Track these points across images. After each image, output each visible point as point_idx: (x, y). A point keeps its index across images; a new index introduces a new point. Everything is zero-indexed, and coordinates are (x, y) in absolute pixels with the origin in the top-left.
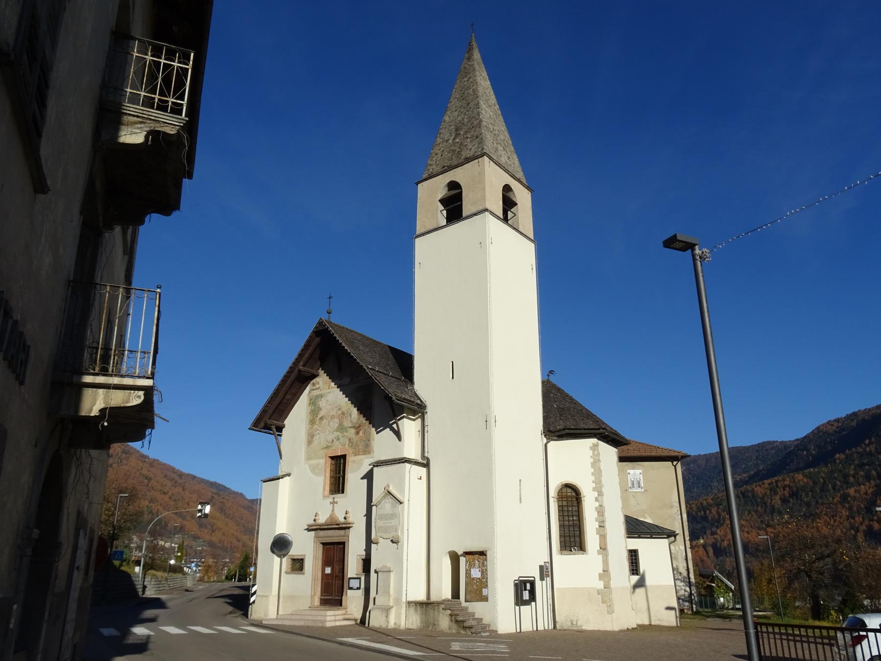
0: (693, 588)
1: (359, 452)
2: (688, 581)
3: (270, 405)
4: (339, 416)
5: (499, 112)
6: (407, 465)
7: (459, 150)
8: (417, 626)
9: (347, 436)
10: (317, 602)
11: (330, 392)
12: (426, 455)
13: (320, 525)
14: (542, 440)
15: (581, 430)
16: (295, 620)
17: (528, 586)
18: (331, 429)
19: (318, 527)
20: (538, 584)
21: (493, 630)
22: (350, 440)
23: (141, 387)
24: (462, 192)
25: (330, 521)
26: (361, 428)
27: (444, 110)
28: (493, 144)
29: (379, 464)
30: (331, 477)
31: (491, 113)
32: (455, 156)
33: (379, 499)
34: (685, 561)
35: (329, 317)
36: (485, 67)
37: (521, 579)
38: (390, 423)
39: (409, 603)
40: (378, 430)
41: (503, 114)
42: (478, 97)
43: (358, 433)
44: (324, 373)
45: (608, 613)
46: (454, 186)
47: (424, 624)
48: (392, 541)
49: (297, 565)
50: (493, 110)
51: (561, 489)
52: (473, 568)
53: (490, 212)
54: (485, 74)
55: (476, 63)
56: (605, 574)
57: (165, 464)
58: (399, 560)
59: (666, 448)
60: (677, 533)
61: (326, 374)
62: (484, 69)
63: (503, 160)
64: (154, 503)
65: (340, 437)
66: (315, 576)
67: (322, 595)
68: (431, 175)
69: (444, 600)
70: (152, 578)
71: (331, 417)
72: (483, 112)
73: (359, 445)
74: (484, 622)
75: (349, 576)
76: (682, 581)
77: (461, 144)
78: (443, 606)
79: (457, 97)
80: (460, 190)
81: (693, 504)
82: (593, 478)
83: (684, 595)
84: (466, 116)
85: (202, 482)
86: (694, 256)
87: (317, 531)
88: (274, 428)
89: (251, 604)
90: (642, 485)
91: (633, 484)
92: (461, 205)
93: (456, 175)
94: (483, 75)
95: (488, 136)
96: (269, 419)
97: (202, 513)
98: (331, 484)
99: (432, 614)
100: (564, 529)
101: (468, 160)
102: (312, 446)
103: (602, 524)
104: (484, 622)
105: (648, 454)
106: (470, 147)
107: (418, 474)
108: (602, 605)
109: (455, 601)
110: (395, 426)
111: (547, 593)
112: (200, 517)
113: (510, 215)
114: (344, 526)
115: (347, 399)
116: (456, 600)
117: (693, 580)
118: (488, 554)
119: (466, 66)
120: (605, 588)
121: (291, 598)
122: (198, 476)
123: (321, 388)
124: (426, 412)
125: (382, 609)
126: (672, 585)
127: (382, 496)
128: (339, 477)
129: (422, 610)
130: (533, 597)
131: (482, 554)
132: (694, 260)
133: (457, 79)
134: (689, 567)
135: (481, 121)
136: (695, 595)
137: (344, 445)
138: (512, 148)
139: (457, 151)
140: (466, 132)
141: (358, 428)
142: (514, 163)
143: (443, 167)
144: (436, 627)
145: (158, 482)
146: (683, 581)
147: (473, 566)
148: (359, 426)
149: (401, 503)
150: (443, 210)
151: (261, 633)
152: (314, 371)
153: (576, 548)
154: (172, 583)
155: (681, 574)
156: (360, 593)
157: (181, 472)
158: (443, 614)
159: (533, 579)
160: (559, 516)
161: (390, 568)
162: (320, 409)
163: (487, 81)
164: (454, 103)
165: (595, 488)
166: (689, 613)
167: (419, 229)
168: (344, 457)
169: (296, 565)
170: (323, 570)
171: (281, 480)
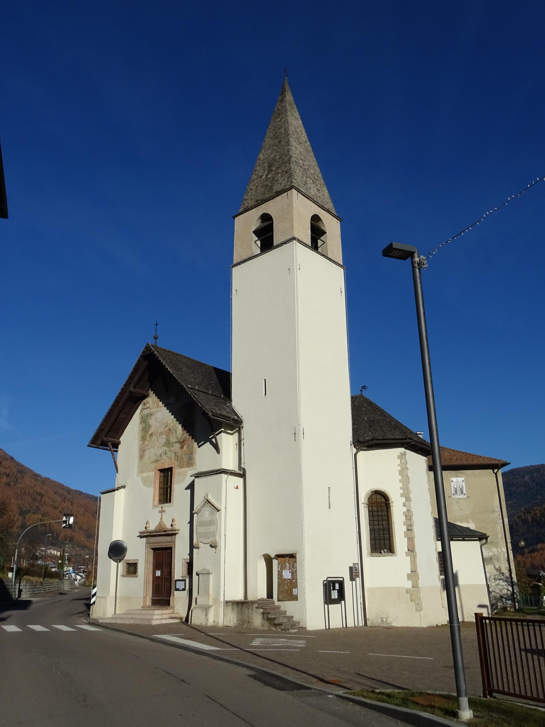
0: (516, 587)
1: (183, 465)
2: (510, 580)
3: (105, 424)
4: (167, 432)
5: (310, 149)
6: (224, 476)
7: (271, 184)
8: (234, 623)
9: (173, 450)
10: (149, 602)
11: (158, 411)
12: (243, 466)
13: (150, 532)
14: (352, 450)
15: (389, 440)
16: (126, 618)
17: (337, 586)
18: (160, 444)
19: (148, 534)
20: (348, 585)
21: (302, 627)
22: (175, 453)
23: (396, 447)
24: (273, 222)
25: (158, 529)
26: (185, 442)
27: (259, 149)
28: (303, 178)
29: (199, 475)
30: (160, 488)
31: (302, 150)
32: (267, 191)
33: (199, 507)
34: (507, 562)
35: (156, 342)
36: (297, 108)
37: (329, 579)
38: (210, 437)
39: (227, 602)
40: (199, 444)
41: (314, 150)
42: (288, 135)
43: (182, 447)
44: (153, 394)
45: (417, 610)
46: (266, 218)
47: (240, 622)
48: (211, 546)
49: (131, 568)
50: (303, 147)
51: (371, 496)
52: (284, 570)
53: (298, 240)
54: (297, 114)
55: (288, 105)
56: (413, 574)
57: (55, 482)
58: (217, 563)
59: (487, 457)
60: (487, 535)
61: (155, 394)
62: (296, 109)
63: (313, 192)
64: (46, 517)
65: (167, 451)
66: (147, 579)
67: (153, 596)
68: (247, 209)
69: (259, 600)
70: (27, 583)
71: (160, 434)
72: (293, 149)
73: (183, 458)
74: (294, 619)
75: (175, 579)
76: (504, 581)
77: (273, 179)
78: (256, 605)
79: (271, 136)
80: (271, 222)
81: (537, 510)
82: (218, 474)
83: (507, 594)
84: (278, 153)
85: (88, 497)
86: (413, 263)
87: (147, 538)
88: (110, 444)
89: (92, 605)
90: (465, 492)
91: (456, 491)
92: (273, 235)
93: (268, 208)
94: (295, 115)
95: (298, 171)
96: (106, 437)
97: (66, 524)
98: (160, 494)
99: (246, 613)
100: (374, 532)
101: (279, 193)
102: (143, 460)
103: (409, 528)
104: (294, 619)
105: (470, 462)
106: (280, 182)
107: (234, 483)
108: (410, 603)
109: (269, 600)
110: (213, 440)
111: (356, 592)
112: (65, 527)
113: (320, 243)
114: (170, 532)
115: (173, 416)
116: (270, 599)
117: (515, 579)
118: (297, 556)
119: (280, 107)
120: (413, 587)
121: (127, 599)
122: (84, 491)
123: (151, 407)
124: (243, 427)
125: (202, 608)
126: (485, 584)
127: (202, 504)
128: (167, 488)
129: (239, 609)
130: (342, 596)
131: (292, 556)
132: (413, 267)
133: (271, 120)
134: (511, 568)
135: (291, 157)
136: (517, 593)
137: (171, 459)
138: (322, 181)
139: (269, 186)
140: (278, 168)
141: (182, 443)
142: (323, 195)
143: (257, 201)
144: (251, 624)
145: (49, 498)
146: (506, 581)
147: (284, 568)
148: (183, 441)
149: (218, 511)
150: (257, 241)
151: (89, 631)
152: (144, 392)
153: (385, 550)
154: (47, 587)
155: (503, 574)
156: (186, 593)
157: (70, 489)
158: (256, 612)
159: (342, 579)
160: (369, 520)
161: (209, 570)
162: (150, 426)
163: (299, 120)
164: (268, 141)
165: (402, 494)
166: (512, 610)
167: (236, 260)
168: (171, 469)
169: (130, 569)
170: (154, 573)
171: (116, 491)
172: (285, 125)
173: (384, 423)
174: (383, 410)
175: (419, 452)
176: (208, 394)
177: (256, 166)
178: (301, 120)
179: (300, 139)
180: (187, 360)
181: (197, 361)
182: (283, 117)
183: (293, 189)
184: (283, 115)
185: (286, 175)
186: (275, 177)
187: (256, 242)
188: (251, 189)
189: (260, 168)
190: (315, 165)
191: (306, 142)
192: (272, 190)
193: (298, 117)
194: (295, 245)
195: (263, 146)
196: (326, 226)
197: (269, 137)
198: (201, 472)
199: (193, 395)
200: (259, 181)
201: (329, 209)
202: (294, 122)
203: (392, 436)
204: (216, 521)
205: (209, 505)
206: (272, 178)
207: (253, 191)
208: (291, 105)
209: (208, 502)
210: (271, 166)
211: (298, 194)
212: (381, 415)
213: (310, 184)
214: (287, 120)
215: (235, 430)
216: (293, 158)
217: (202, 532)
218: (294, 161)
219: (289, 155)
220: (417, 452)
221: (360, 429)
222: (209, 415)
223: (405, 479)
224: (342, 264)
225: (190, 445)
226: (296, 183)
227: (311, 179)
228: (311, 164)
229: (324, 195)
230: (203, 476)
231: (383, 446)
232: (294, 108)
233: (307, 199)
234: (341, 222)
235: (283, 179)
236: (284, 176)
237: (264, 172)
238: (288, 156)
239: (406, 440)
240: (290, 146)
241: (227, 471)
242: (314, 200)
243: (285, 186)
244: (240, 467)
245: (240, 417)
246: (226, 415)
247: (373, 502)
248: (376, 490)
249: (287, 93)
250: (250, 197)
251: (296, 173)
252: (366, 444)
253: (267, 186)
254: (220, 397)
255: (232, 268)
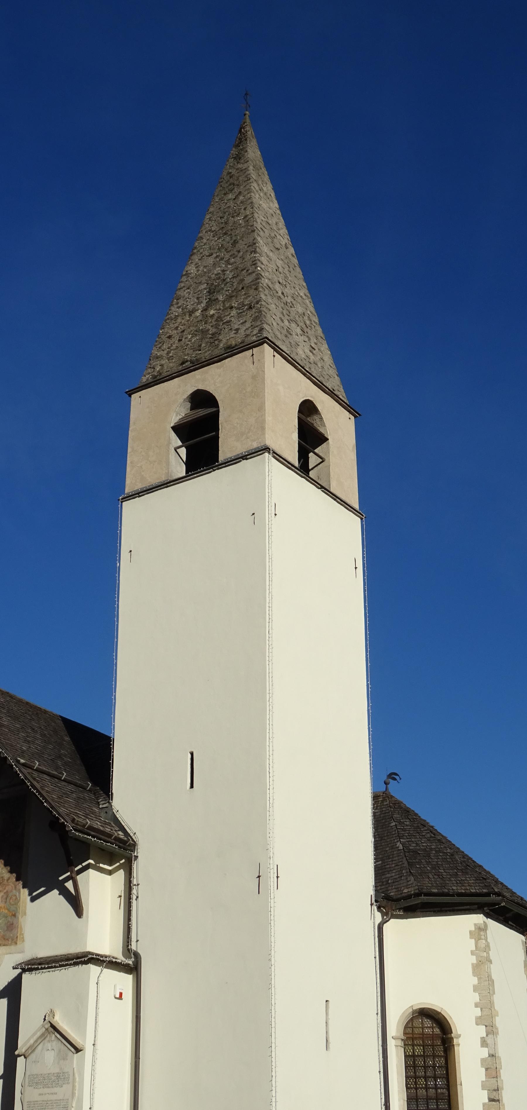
5: (295, 261)
6: (94, 969)
7: (214, 330)
12: (133, 947)
15: (453, 895)
24: (218, 411)
31: (280, 263)
32: (207, 343)
33: (32, 1041)
38: (61, 878)
40: (34, 894)
42: (253, 231)
51: (412, 1020)
53: (274, 452)
54: (269, 188)
55: (251, 168)
62: (266, 178)
63: (301, 353)
68: (158, 377)
72: (263, 259)
77: (219, 319)
79: (213, 229)
82: (80, 966)
84: (230, 266)
92: (216, 438)
94: (265, 189)
95: (273, 306)
101: (232, 351)
103: (494, 1095)
106: (236, 327)
119: (233, 171)
127: (39, 1034)
135: (259, 277)
138: (320, 331)
142: (322, 359)
143: (183, 363)
149: (78, 1050)
163: (272, 201)
165: (480, 1017)
167: (131, 484)
172: (245, 209)
173: (440, 857)
174: (432, 827)
175: (510, 923)
176: (59, 779)
177: (181, 289)
178: (276, 201)
179: (275, 240)
180: (8, 698)
181: (27, 703)
182: (240, 193)
183: (265, 345)
184: (242, 187)
185: (250, 313)
186: (225, 316)
187: (177, 450)
188: (168, 335)
189: (189, 293)
190: (304, 297)
191: (287, 248)
192: (216, 342)
193: (270, 195)
194: (267, 464)
195: (196, 248)
196: (327, 425)
197: (210, 231)
198: (37, 959)
199: (29, 781)
200: (188, 321)
201: (333, 390)
202: (264, 205)
203: (458, 888)
204: (71, 1074)
205: (56, 1036)
206: (218, 317)
207: (173, 340)
208: (258, 170)
209: (52, 1030)
210: (214, 292)
211: (274, 356)
212: (431, 839)
213: (297, 336)
214: (250, 198)
215: (118, 864)
216: (263, 279)
217: (37, 1101)
218: (265, 285)
219: (256, 273)
220: (508, 923)
221: (389, 870)
222: (67, 829)
223: (487, 983)
224: (357, 506)
225: (10, 895)
226: (270, 331)
227: (298, 326)
228: (297, 294)
229: (324, 361)
230: (45, 968)
231: (439, 909)
232: (262, 176)
233: (293, 368)
234: (356, 418)
235: (242, 321)
236: (244, 316)
237: (200, 303)
238: (254, 275)
239: (490, 896)
240: (258, 255)
241: (101, 959)
242: (305, 370)
243: (247, 336)
244: (128, 950)
245: (132, 835)
246: (101, 828)
247: (415, 1036)
248: (424, 1009)
249: (250, 144)
250: (166, 352)
251: (270, 310)
252: (404, 904)
253: (204, 332)
254: (85, 788)
255: (122, 502)
